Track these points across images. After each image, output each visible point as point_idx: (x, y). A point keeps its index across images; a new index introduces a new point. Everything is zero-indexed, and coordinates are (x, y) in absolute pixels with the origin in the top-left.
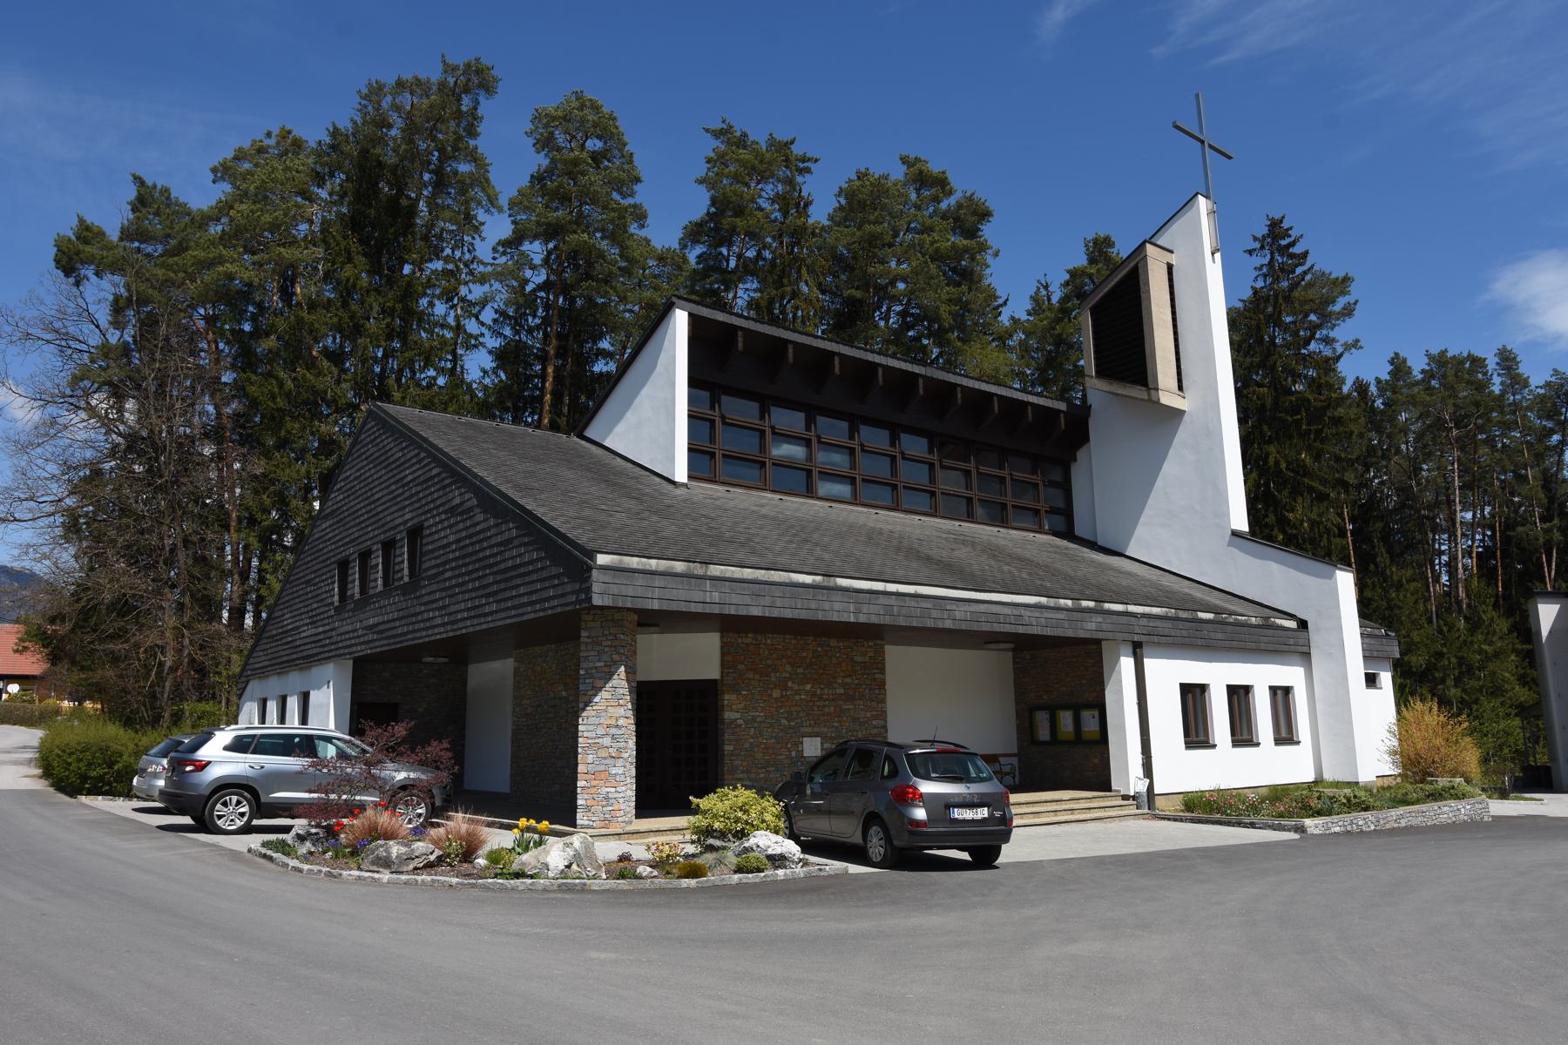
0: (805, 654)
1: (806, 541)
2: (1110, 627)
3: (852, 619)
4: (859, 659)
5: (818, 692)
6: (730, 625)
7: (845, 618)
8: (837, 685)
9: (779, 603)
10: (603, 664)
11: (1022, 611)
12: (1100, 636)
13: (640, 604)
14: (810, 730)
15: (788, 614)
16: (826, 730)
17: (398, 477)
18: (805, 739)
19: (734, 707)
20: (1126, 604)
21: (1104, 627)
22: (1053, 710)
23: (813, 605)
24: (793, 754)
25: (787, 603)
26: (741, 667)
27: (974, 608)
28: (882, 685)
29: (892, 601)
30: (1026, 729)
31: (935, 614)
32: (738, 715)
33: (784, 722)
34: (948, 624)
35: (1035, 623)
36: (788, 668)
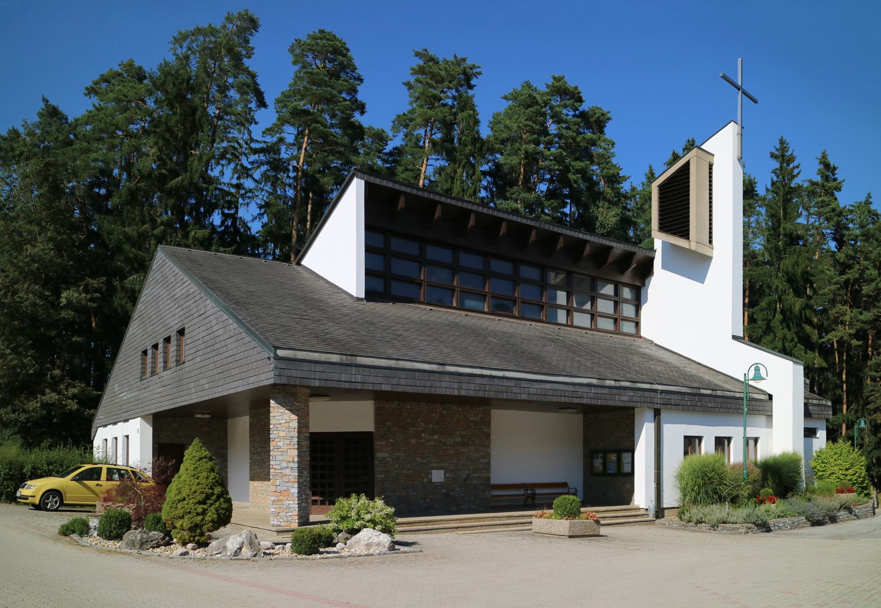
0: (434, 415)
1: (436, 339)
2: (638, 399)
3: (456, 393)
4: (473, 419)
5: (443, 440)
6: (379, 396)
7: (449, 392)
8: (456, 436)
9: (403, 382)
10: (284, 421)
11: (577, 388)
12: (631, 405)
13: (377, 388)
14: (437, 465)
15: (410, 390)
16: (448, 465)
17: (172, 295)
18: (433, 471)
19: (384, 450)
20: (652, 384)
21: (635, 399)
22: (605, 453)
23: (428, 384)
24: (425, 480)
25: (410, 382)
26: (388, 423)
27: (543, 386)
28: (488, 436)
29: (485, 381)
30: (588, 467)
31: (515, 390)
32: (386, 455)
33: (419, 459)
34: (523, 397)
35: (585, 396)
36: (422, 424)
